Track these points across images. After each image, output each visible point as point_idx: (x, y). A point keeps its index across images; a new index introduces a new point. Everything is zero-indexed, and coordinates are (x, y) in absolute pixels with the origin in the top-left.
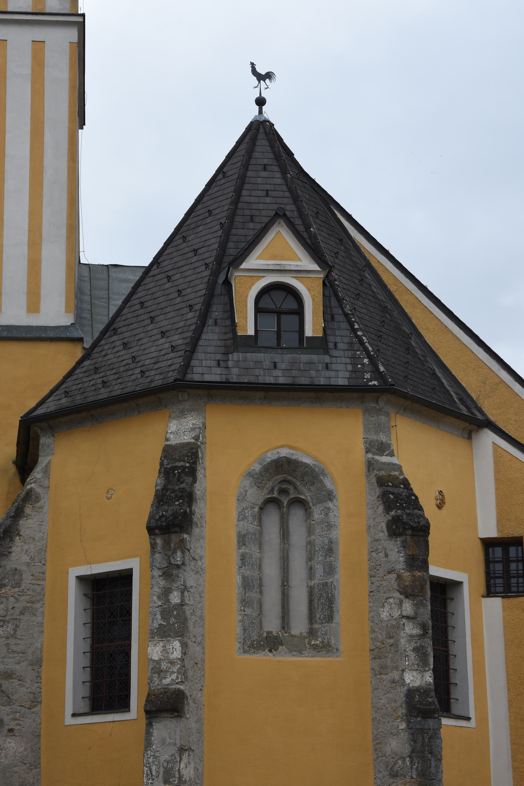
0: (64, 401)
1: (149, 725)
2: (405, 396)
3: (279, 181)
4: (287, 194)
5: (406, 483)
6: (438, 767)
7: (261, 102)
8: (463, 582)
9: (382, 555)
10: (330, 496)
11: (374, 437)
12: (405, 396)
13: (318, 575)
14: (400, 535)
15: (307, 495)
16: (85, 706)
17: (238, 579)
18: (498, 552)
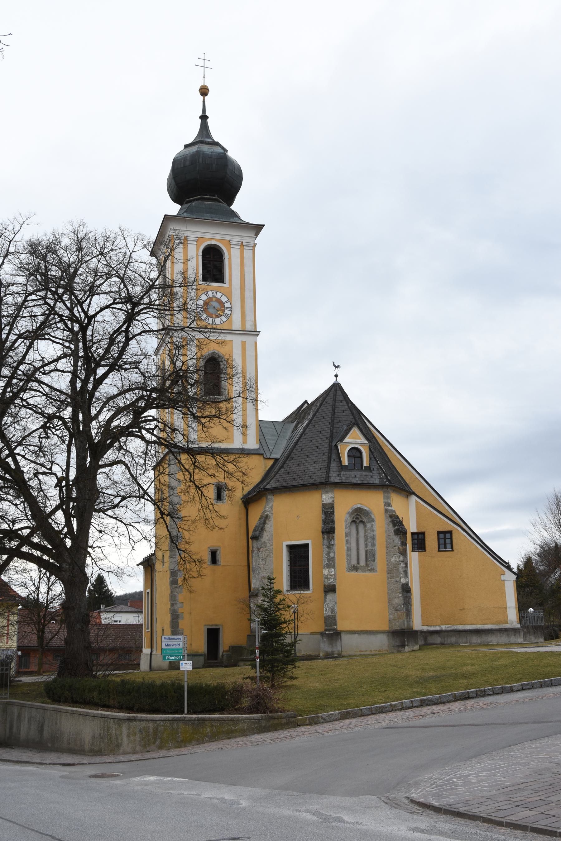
0: (278, 484)
1: (325, 595)
2: (396, 487)
3: (346, 407)
4: (350, 412)
5: (397, 516)
6: (411, 607)
7: (336, 376)
8: (425, 551)
9: (392, 540)
10: (373, 520)
11: (387, 501)
12: (396, 487)
13: (369, 546)
14: (399, 535)
15: (365, 520)
16: (289, 589)
17: (346, 548)
18: (416, 536)
